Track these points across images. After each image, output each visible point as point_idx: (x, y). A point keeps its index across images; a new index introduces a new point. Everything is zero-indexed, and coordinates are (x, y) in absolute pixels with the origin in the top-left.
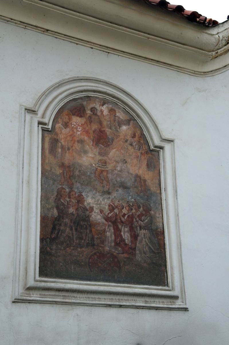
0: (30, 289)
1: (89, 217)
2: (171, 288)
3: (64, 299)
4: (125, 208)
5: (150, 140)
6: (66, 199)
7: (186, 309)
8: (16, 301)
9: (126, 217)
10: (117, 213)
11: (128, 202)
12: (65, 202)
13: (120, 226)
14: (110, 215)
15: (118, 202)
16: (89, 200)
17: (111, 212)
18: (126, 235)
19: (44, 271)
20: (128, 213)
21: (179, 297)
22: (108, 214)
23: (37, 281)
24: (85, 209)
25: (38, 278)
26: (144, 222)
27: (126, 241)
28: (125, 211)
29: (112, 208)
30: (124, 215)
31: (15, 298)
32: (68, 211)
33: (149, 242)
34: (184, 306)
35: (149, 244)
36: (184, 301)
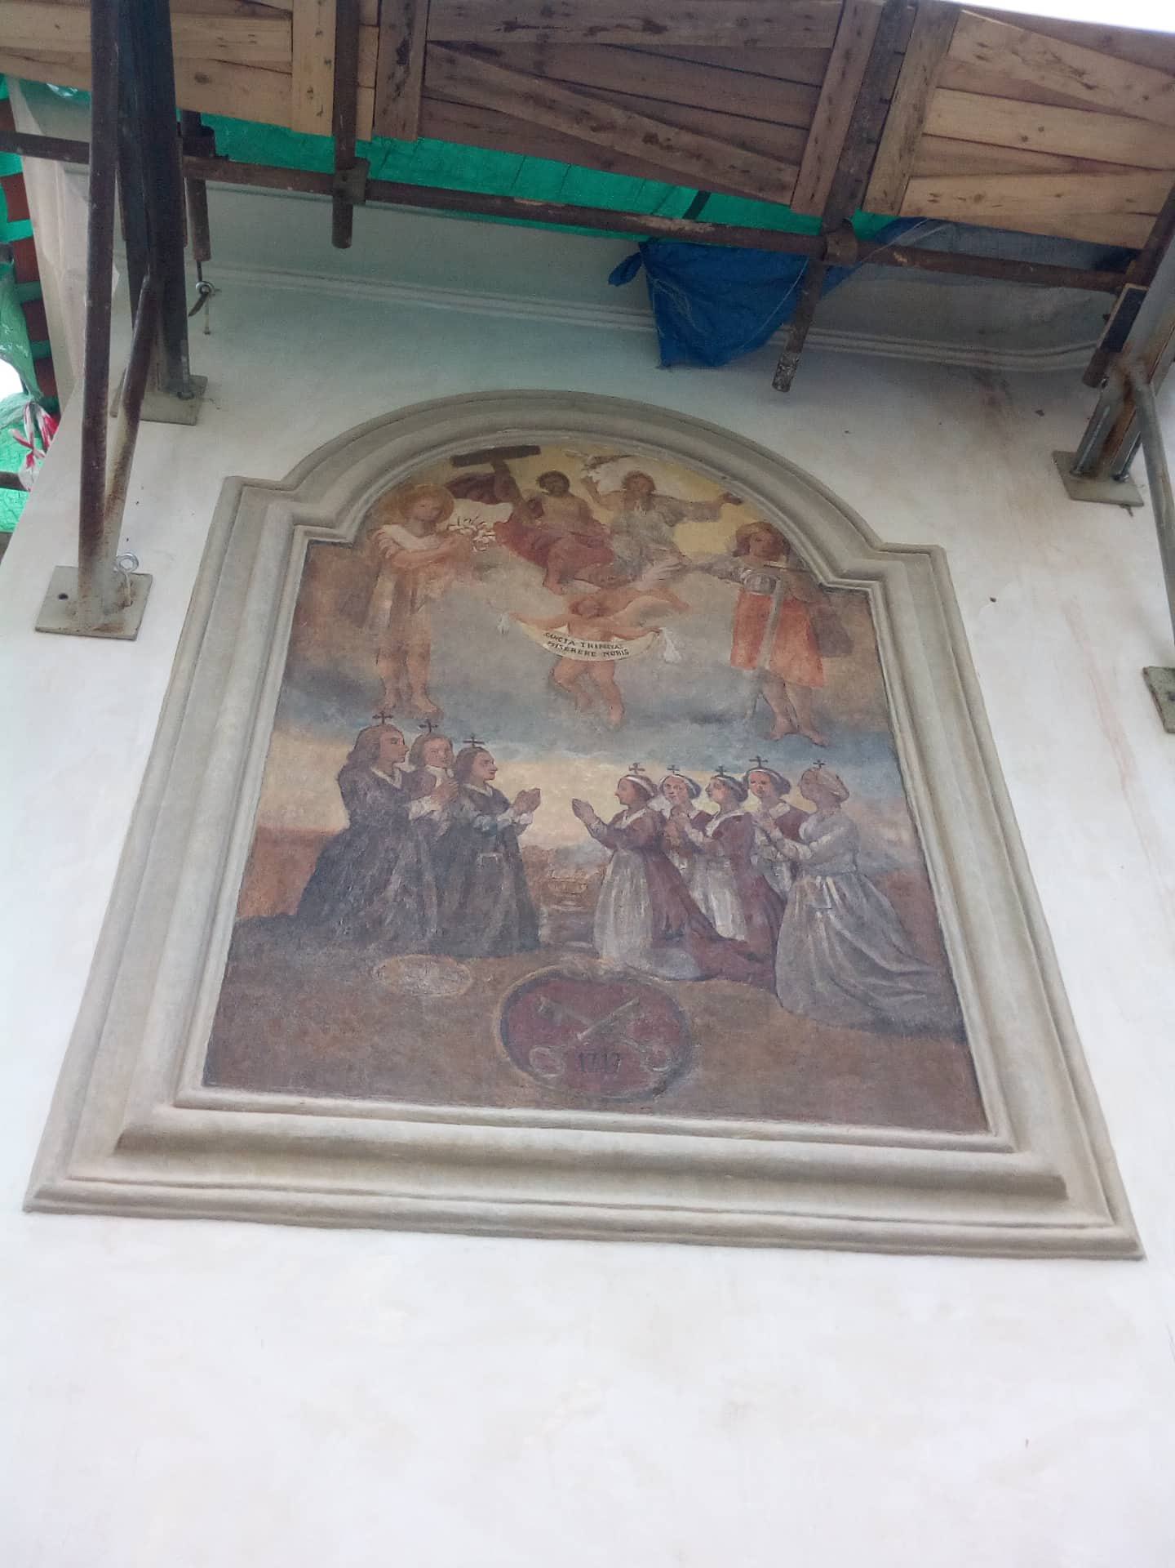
0: (138, 1144)
1: (515, 829)
2: (1003, 1136)
3: (331, 1188)
4: (704, 794)
5: (266, 1179)
6: (398, 765)
7: (1126, 1250)
8: (49, 1201)
9: (711, 829)
10: (667, 814)
11: (721, 770)
12: (392, 776)
13: (682, 866)
14: (626, 822)
15: (669, 773)
16: (513, 772)
17: (631, 811)
18: (725, 914)
19: (218, 1070)
20: (724, 810)
21: (1065, 1177)
22: (618, 817)
23: (878, 577)
24: (498, 801)
25: (193, 1085)
26: (814, 844)
27: (718, 923)
28: (703, 804)
29: (640, 794)
30: (703, 819)
31: (127, 1121)
32: (407, 811)
33: (846, 927)
34: (1112, 1232)
35: (847, 934)
36: (1113, 1205)
